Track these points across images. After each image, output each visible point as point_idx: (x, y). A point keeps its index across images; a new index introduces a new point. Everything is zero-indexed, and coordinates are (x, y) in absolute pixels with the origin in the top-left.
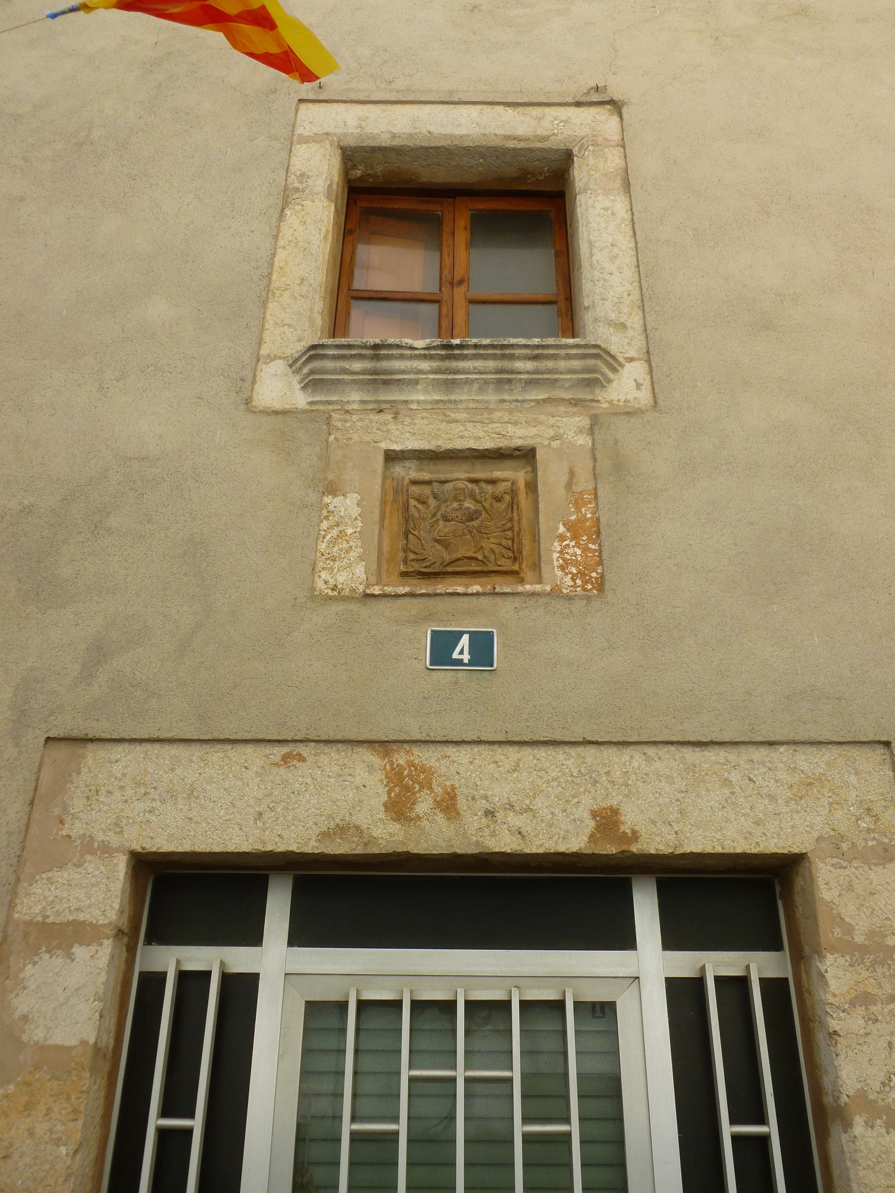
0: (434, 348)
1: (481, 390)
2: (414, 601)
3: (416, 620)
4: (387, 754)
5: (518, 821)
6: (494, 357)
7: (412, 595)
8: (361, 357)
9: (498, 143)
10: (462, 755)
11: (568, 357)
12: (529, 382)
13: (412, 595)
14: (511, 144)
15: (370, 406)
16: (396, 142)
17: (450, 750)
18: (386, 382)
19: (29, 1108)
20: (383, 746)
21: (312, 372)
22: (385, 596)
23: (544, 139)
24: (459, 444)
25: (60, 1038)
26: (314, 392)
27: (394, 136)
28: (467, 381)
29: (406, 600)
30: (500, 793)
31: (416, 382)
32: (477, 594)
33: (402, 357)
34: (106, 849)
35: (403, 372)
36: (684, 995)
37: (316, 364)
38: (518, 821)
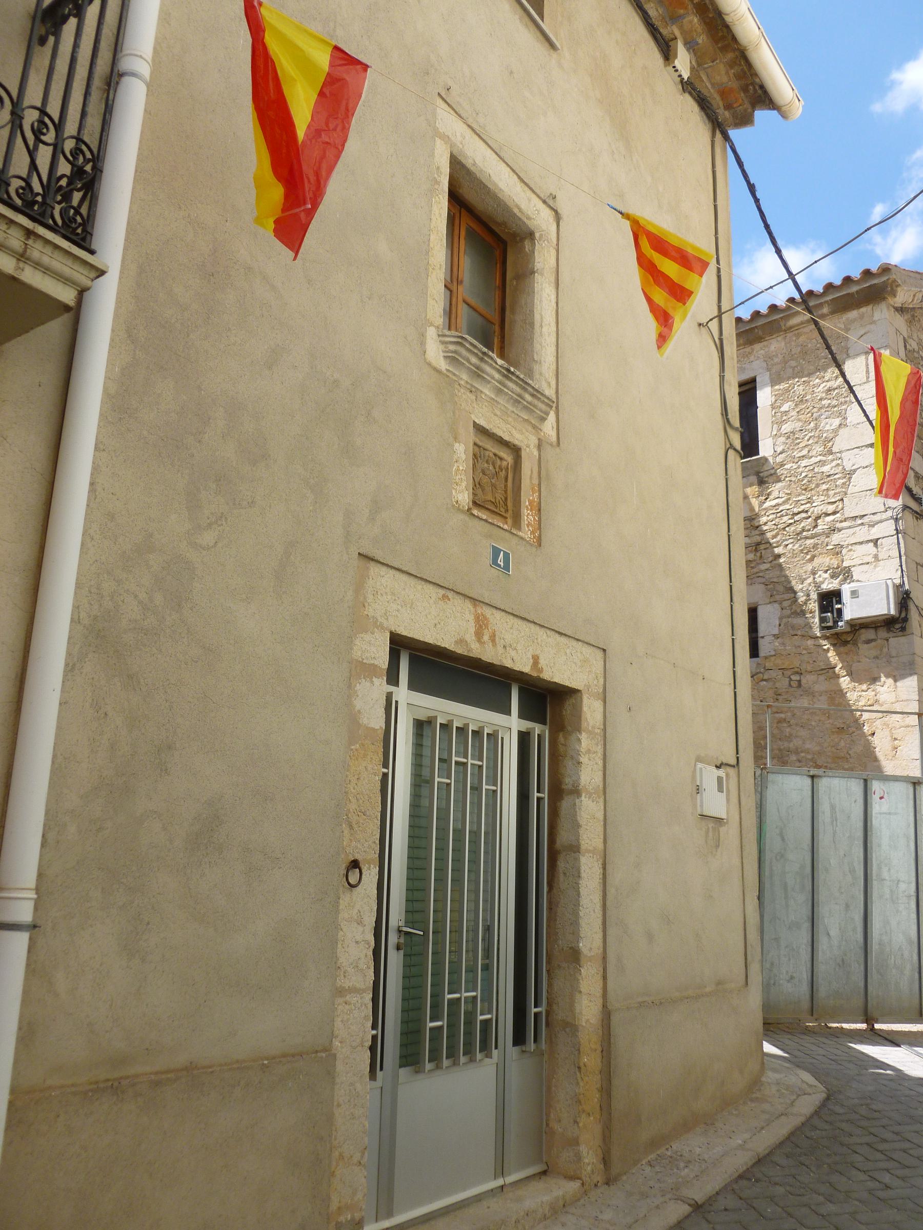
0: (503, 368)
1: (508, 401)
2: (486, 524)
3: (489, 536)
4: (475, 606)
5: (513, 653)
6: (520, 386)
7: (486, 521)
8: (476, 355)
9: (510, 204)
10: (498, 614)
11: (543, 402)
12: (525, 407)
13: (486, 521)
14: (516, 211)
15: (469, 386)
16: (472, 169)
17: (494, 611)
18: (479, 376)
19: (365, 756)
20: (474, 601)
21: (455, 352)
22: (478, 517)
23: (529, 218)
24: (500, 433)
25: (372, 725)
26: (450, 363)
27: (474, 164)
28: (506, 394)
29: (483, 522)
30: (509, 637)
31: (489, 382)
32: (506, 530)
33: (491, 365)
34: (382, 627)
35: (488, 375)
36: (524, 738)
37: (458, 348)
38: (513, 653)
